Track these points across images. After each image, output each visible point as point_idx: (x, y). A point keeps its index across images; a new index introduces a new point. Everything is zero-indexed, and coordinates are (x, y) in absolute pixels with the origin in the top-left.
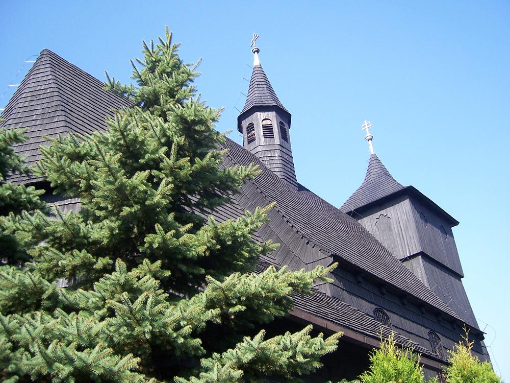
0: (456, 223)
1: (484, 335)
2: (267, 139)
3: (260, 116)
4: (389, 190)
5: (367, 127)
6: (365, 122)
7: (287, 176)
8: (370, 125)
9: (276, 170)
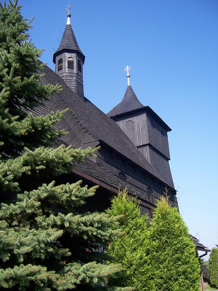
0: (170, 130)
1: (177, 192)
3: (67, 55)
4: (135, 107)
5: (128, 70)
6: (127, 66)
7: (79, 92)
8: (130, 69)
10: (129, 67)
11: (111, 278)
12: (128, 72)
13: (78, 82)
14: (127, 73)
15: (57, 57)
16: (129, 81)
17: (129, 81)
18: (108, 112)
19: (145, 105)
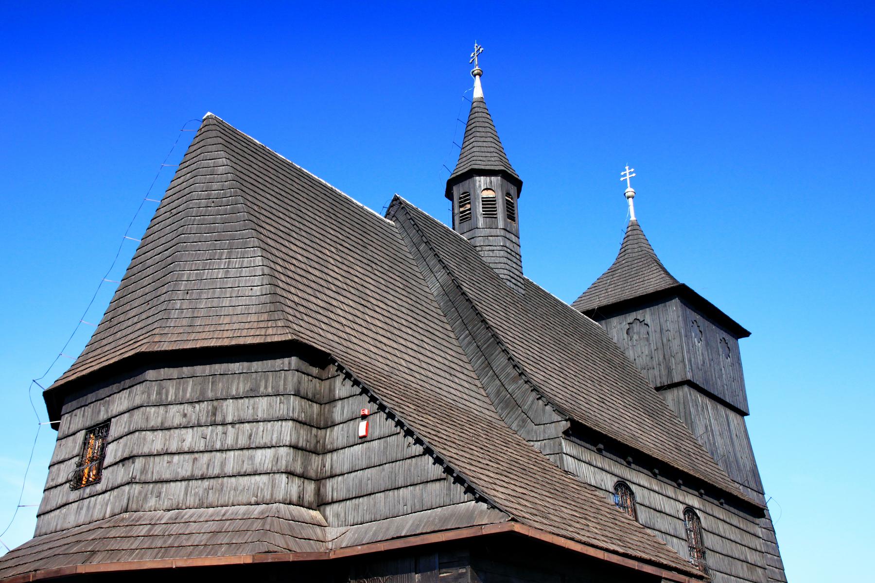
0: (746, 334)
2: (488, 219)
3: (481, 181)
4: (653, 283)
5: (628, 177)
6: (627, 168)
7: (511, 274)
8: (634, 175)
9: (499, 266)
10: (632, 170)
11: (652, 314)
12: (629, 185)
13: (509, 251)
15: (455, 188)
18: (584, 291)
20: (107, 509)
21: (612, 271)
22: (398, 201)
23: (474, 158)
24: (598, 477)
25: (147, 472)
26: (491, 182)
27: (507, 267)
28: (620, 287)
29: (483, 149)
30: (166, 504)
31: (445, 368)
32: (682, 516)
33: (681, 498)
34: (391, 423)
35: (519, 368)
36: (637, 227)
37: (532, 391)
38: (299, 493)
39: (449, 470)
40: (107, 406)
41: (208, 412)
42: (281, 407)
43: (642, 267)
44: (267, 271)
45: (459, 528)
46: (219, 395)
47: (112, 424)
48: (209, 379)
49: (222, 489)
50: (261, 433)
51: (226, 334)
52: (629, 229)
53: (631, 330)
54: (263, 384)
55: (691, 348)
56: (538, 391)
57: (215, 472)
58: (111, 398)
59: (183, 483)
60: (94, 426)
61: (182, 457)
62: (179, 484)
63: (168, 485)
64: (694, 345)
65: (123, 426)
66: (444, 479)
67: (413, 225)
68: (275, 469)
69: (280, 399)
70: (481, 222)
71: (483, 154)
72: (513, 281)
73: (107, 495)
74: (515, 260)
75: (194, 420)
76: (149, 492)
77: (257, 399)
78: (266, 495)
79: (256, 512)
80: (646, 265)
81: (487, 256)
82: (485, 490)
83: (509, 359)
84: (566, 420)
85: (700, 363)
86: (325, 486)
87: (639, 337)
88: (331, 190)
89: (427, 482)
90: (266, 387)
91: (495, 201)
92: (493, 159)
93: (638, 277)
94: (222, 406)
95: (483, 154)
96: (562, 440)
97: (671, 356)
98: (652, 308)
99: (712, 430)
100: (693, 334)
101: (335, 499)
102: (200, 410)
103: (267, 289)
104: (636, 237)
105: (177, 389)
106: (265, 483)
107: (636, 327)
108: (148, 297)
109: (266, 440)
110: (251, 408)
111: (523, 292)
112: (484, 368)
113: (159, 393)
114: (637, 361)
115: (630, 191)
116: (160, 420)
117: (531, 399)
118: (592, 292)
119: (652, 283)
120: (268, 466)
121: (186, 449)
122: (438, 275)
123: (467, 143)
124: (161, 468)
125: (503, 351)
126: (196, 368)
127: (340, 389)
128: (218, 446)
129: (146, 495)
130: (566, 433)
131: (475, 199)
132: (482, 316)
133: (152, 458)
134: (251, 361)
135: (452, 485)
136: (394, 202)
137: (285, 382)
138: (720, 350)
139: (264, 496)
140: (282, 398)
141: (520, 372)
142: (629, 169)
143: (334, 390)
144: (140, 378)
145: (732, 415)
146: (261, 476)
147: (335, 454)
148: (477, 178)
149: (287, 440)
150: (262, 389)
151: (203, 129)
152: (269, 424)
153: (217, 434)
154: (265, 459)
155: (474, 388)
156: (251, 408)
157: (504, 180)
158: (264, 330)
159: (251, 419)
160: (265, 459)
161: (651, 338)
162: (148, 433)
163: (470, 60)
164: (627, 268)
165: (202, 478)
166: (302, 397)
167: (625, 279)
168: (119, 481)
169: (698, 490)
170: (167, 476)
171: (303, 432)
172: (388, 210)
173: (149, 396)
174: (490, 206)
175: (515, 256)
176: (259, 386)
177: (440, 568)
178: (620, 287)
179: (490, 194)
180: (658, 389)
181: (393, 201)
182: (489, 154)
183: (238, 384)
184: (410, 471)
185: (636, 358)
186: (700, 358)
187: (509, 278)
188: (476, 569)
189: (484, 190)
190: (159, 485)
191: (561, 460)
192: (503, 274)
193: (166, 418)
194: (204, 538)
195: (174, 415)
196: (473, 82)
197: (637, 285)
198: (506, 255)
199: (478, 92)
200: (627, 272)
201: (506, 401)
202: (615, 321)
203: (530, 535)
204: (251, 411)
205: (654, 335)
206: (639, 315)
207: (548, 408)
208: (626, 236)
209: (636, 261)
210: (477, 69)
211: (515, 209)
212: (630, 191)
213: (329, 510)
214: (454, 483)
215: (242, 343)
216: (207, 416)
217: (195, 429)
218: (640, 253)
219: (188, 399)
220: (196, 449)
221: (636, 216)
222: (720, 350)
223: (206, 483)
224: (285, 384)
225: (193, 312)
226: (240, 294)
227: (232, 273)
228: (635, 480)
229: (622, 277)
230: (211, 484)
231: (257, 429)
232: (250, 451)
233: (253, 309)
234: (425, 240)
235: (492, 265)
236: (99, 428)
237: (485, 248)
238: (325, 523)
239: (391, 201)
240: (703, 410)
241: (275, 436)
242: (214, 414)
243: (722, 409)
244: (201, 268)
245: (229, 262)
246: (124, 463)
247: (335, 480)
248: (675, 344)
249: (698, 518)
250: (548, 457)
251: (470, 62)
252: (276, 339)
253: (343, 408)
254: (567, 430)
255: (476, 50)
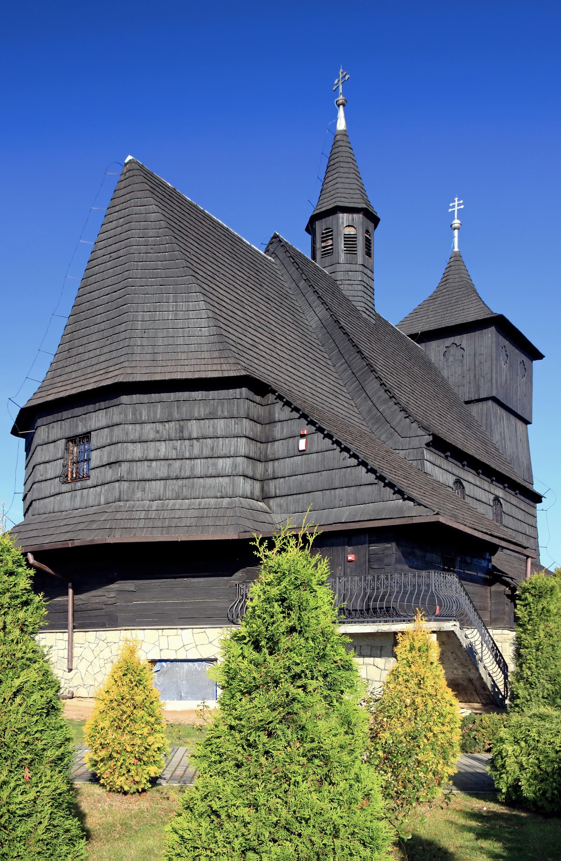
0: (540, 356)
1: (543, 499)
2: (348, 255)
3: (344, 218)
5: (456, 208)
6: (456, 199)
8: (462, 207)
9: (357, 299)
10: (461, 202)
13: (365, 285)
14: (454, 219)
16: (456, 240)
17: (456, 240)
18: (401, 319)
19: (497, 310)
20: (100, 499)
21: (433, 298)
22: (278, 239)
23: (338, 195)
24: (444, 477)
25: (132, 473)
26: (353, 220)
27: (364, 300)
28: (441, 313)
29: (346, 186)
30: (150, 496)
31: (332, 392)
32: (492, 504)
33: (492, 491)
34: (328, 441)
35: (390, 392)
36: (460, 258)
37: (400, 411)
38: (251, 490)
39: (381, 478)
40: (84, 422)
41: (176, 430)
42: (234, 427)
43: (461, 296)
44: (211, 314)
45: (392, 518)
46: (184, 417)
47: (92, 436)
48: (174, 404)
49: (193, 486)
50: (221, 447)
51: (187, 368)
52: (452, 259)
53: (447, 353)
54: (220, 408)
55: (499, 370)
56: (406, 412)
57: (186, 474)
58: (87, 415)
59: (162, 481)
60: (74, 437)
61: (158, 462)
62: (158, 482)
63: (150, 483)
64: (501, 367)
65: (105, 438)
66: (376, 484)
67: (293, 263)
68: (234, 473)
69: (235, 421)
70: (342, 258)
71: (347, 191)
72: (368, 312)
73: (98, 489)
74: (370, 294)
75: (165, 435)
76: (136, 488)
77: (216, 421)
78: (228, 491)
79: (224, 503)
80: (466, 295)
81: (346, 291)
82: (412, 493)
83: (381, 385)
84: (429, 435)
85: (504, 382)
86: (269, 485)
87: (454, 359)
88: (227, 230)
89: (361, 485)
90: (222, 411)
91: (355, 238)
92: (355, 196)
93: (458, 306)
94: (187, 425)
95: (347, 191)
96: (425, 451)
97: (482, 376)
98: (469, 334)
99: (504, 436)
100: (501, 358)
101: (278, 494)
102: (169, 428)
103: (214, 330)
104: (457, 268)
105: (149, 411)
106: (227, 483)
107: (453, 350)
108: (106, 333)
109: (225, 452)
110: (211, 427)
111: (374, 322)
112: (358, 391)
113: (134, 414)
114: (450, 379)
115: (456, 222)
116: (137, 434)
117: (399, 417)
118: (414, 318)
119: (471, 312)
120: (228, 470)
121: (162, 457)
122: (317, 310)
123: (330, 179)
124: (142, 470)
125: (376, 378)
126: (162, 394)
127: (279, 414)
128: (187, 455)
129: (133, 490)
130: (428, 445)
131: (338, 235)
132: (358, 348)
133: (134, 463)
134: (209, 391)
135: (382, 488)
136: (274, 240)
137: (237, 407)
138: (519, 370)
139: (227, 492)
140: (236, 420)
141: (391, 395)
142: (458, 200)
143: (274, 414)
144: (115, 401)
145: (520, 424)
146: (224, 478)
147: (276, 462)
148: (341, 215)
149: (242, 451)
150: (219, 413)
151: (127, 174)
152: (227, 440)
153: (185, 446)
154: (224, 465)
155: (351, 407)
156: (211, 427)
157: (365, 218)
158: (219, 366)
159: (212, 436)
160: (224, 465)
161: (465, 361)
162: (129, 444)
163: (333, 87)
164: (447, 297)
165: (177, 478)
166: (251, 420)
167: (445, 306)
168: (108, 479)
169: (503, 484)
170: (148, 476)
171: (252, 444)
172: (268, 247)
173: (126, 416)
174: (351, 243)
175: (369, 290)
176: (217, 411)
177: (369, 544)
178: (441, 313)
179: (352, 231)
180: (467, 403)
181: (272, 238)
182: (351, 191)
183: (199, 408)
184: (345, 477)
185: (450, 376)
186: (504, 378)
187: (364, 310)
188: (398, 545)
189: (346, 226)
190: (143, 483)
191: (423, 465)
192: (360, 306)
193: (142, 433)
194: (193, 522)
195: (149, 431)
196: (337, 112)
197: (457, 313)
198: (363, 289)
199: (341, 125)
200: (447, 300)
201: (377, 418)
202: (434, 344)
203: (447, 524)
204: (211, 429)
205: (468, 357)
206: (456, 339)
207: (414, 425)
208: (448, 266)
209: (456, 291)
210: (341, 98)
211: (372, 245)
212: (456, 222)
213: (272, 502)
214: (384, 487)
215: (204, 377)
216: (176, 433)
217: (167, 442)
218: (461, 283)
219: (159, 419)
220: (170, 458)
221: (459, 247)
222: (519, 370)
223: (180, 482)
224: (238, 410)
225: (153, 349)
226: (191, 334)
227: (181, 315)
228: (467, 479)
229: (442, 304)
230: (184, 483)
231: (218, 443)
232: (213, 459)
233: (205, 347)
234: (305, 278)
235: (350, 298)
236: (80, 438)
237: (344, 282)
238: (271, 512)
239: (270, 239)
240: (500, 421)
241: (232, 449)
242: (182, 431)
243: (512, 418)
244: (152, 310)
245: (176, 305)
246: (110, 465)
247: (277, 481)
248: (486, 367)
249: (501, 504)
250: (411, 462)
251: (334, 89)
252: (232, 374)
253: (282, 429)
254: (429, 443)
255: (341, 77)
